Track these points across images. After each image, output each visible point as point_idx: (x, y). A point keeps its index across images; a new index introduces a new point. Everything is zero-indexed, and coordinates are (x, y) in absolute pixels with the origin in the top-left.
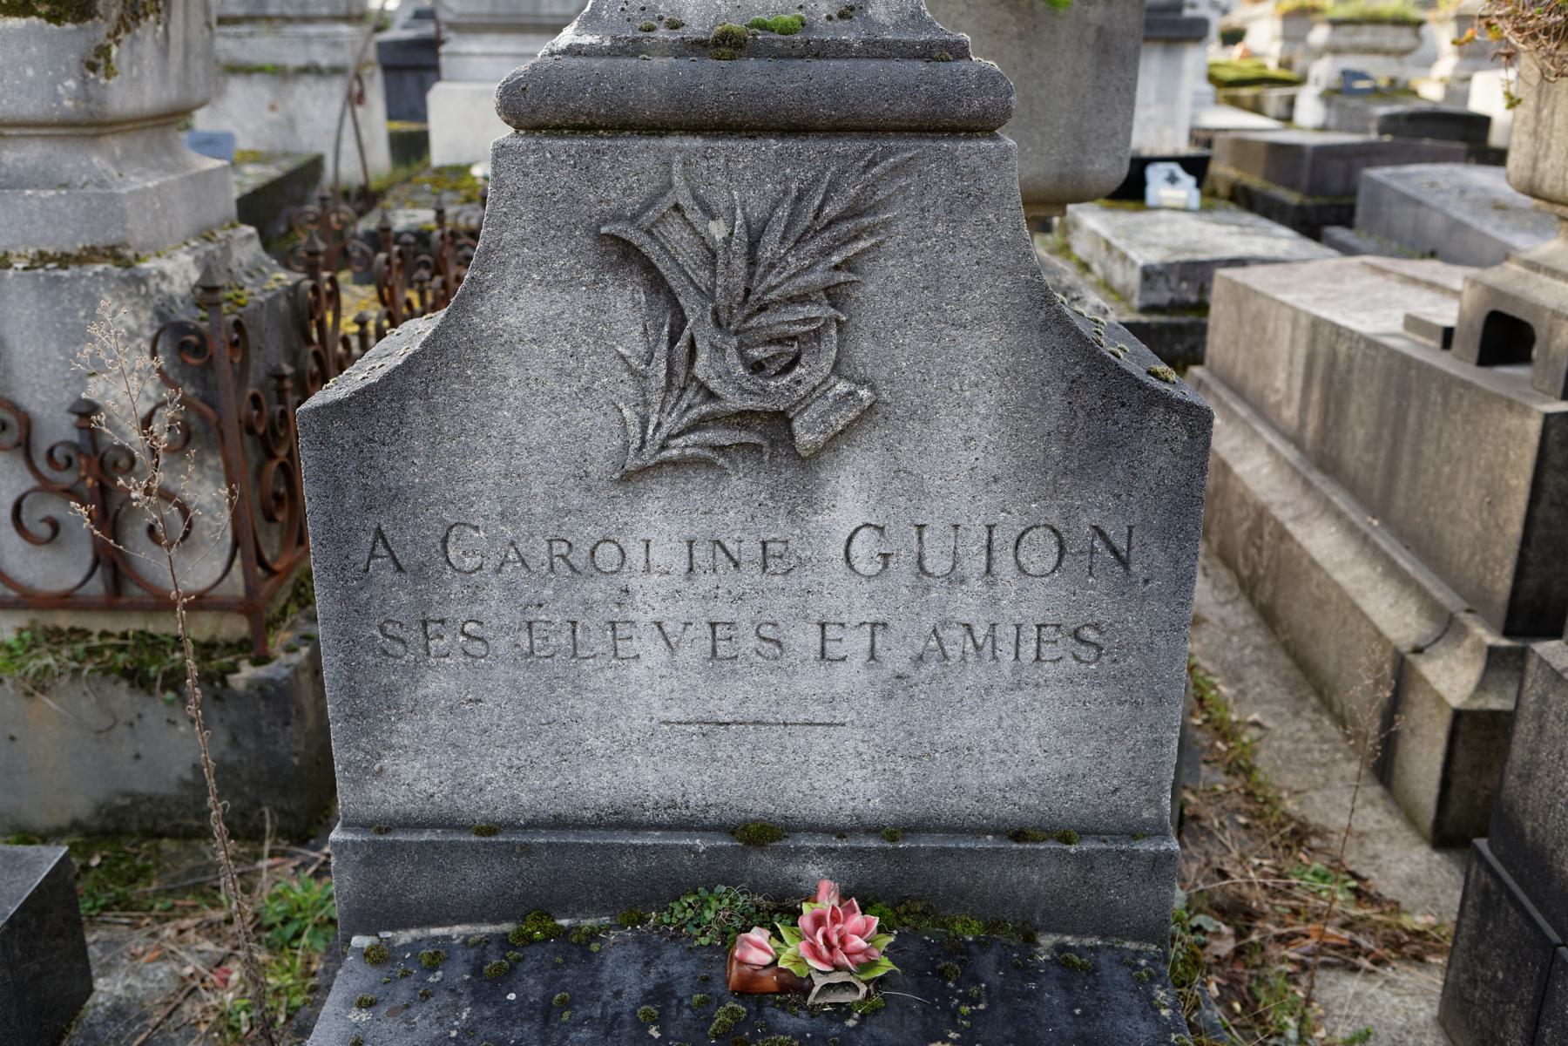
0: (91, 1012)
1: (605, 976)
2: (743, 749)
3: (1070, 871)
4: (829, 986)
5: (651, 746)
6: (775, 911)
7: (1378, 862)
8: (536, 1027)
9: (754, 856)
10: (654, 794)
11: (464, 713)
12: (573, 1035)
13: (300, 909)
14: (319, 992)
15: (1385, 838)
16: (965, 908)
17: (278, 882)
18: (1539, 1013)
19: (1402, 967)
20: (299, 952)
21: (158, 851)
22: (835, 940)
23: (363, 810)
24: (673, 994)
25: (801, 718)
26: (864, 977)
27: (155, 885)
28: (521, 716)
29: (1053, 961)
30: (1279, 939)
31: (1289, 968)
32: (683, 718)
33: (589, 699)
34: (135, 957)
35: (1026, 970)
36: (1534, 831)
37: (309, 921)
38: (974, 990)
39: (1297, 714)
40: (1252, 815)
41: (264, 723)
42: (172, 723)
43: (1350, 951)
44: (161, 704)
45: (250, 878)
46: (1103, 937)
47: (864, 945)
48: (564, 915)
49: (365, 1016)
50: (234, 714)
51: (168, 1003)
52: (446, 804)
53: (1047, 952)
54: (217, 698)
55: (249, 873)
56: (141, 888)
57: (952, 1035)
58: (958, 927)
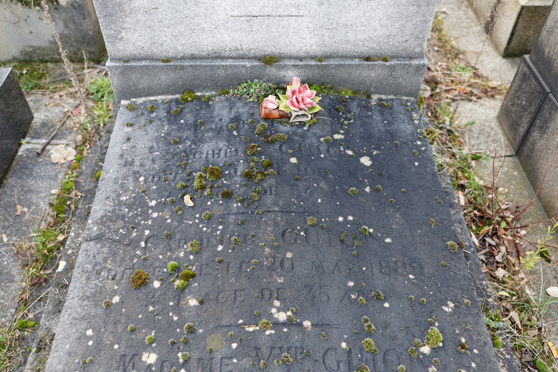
0: (35, 125)
1: (215, 113)
2: (263, 27)
3: (386, 72)
4: (297, 116)
5: (227, 26)
6: (276, 88)
7: (483, 63)
8: (192, 132)
9: (268, 68)
10: (229, 45)
11: (151, 14)
12: (206, 135)
13: (102, 87)
14: (113, 118)
15: (486, 54)
16: (346, 86)
17: (92, 78)
18: (536, 116)
19: (486, 99)
20: (104, 103)
21: (47, 68)
22: (300, 100)
23: (117, 53)
24: (241, 119)
25: (286, 13)
26: (310, 112)
27: (48, 80)
28: (175, 15)
29: (378, 104)
30: (446, 91)
31: (448, 101)
32: (239, 14)
33: (201, 7)
34: (46, 105)
35: (367, 108)
36: (549, 52)
37: (106, 91)
38: (349, 116)
39: (459, 8)
40: (440, 47)
41: (76, 18)
42: (41, 19)
43: (470, 94)
44: (35, 12)
45: (82, 76)
46: (395, 95)
47: (311, 101)
48: (199, 91)
49: (130, 129)
50: (64, 15)
51: (61, 121)
52: (149, 51)
53: (375, 101)
54: (56, 9)
55: (82, 75)
56: (43, 81)
57: (342, 132)
58: (343, 93)
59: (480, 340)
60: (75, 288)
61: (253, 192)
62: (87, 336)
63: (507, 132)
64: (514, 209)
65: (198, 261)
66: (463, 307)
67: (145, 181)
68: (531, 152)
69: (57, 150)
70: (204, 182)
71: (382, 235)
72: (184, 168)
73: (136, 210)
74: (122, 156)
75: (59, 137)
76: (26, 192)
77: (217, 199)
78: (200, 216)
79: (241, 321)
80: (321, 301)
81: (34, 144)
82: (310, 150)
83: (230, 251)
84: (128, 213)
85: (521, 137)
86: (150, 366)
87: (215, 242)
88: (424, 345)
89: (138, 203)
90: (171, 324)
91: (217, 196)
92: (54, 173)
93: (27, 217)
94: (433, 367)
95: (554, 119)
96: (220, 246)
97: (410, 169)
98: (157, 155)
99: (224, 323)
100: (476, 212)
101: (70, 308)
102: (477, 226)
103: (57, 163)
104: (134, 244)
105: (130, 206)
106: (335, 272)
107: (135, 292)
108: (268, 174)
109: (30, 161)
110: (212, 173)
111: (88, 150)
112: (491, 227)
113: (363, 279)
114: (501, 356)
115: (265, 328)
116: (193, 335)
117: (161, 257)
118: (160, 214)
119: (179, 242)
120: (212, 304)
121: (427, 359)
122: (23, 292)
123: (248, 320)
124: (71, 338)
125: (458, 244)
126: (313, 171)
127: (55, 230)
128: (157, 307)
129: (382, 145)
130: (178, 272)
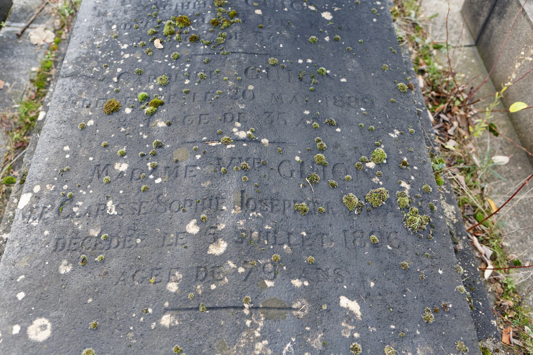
0: (14, 10)
18: (496, 3)
59: (420, 160)
60: (52, 114)
61: (219, 36)
62: (64, 151)
63: (469, 25)
64: (468, 90)
65: (166, 92)
66: (408, 134)
67: (118, 28)
68: (489, 39)
69: (36, 32)
70: (173, 29)
71: (338, 75)
72: (155, 18)
73: (109, 52)
74: (95, 8)
75: (38, 21)
76: (7, 69)
77: (185, 42)
78: (169, 56)
79: (205, 138)
80: (279, 124)
81: (14, 27)
82: (274, 4)
83: (196, 84)
84: (101, 55)
85: (481, 26)
86: (122, 173)
87: (182, 77)
88: (370, 162)
89: (112, 46)
90: (140, 140)
91: (185, 40)
92: (34, 53)
93: (9, 91)
94: (376, 178)
95: (511, 3)
96: (187, 80)
97: (368, 24)
98: (129, 7)
99: (190, 139)
100: (434, 93)
101: (48, 130)
102: (433, 105)
103: (37, 45)
104: (107, 79)
105: (103, 49)
106: (293, 102)
107: (108, 117)
108: (233, 23)
109: (10, 42)
110: (181, 21)
111: (66, 33)
112: (446, 105)
113: (318, 109)
114: (442, 192)
115: (227, 143)
116: (161, 149)
117: (132, 89)
118: (132, 55)
119: (149, 78)
120: (179, 126)
121: (371, 172)
122: (8, 155)
123: (211, 137)
124: (49, 153)
125: (408, 86)
126: (277, 21)
127: (37, 102)
128: (128, 128)
129: (343, 3)
130: (148, 101)
